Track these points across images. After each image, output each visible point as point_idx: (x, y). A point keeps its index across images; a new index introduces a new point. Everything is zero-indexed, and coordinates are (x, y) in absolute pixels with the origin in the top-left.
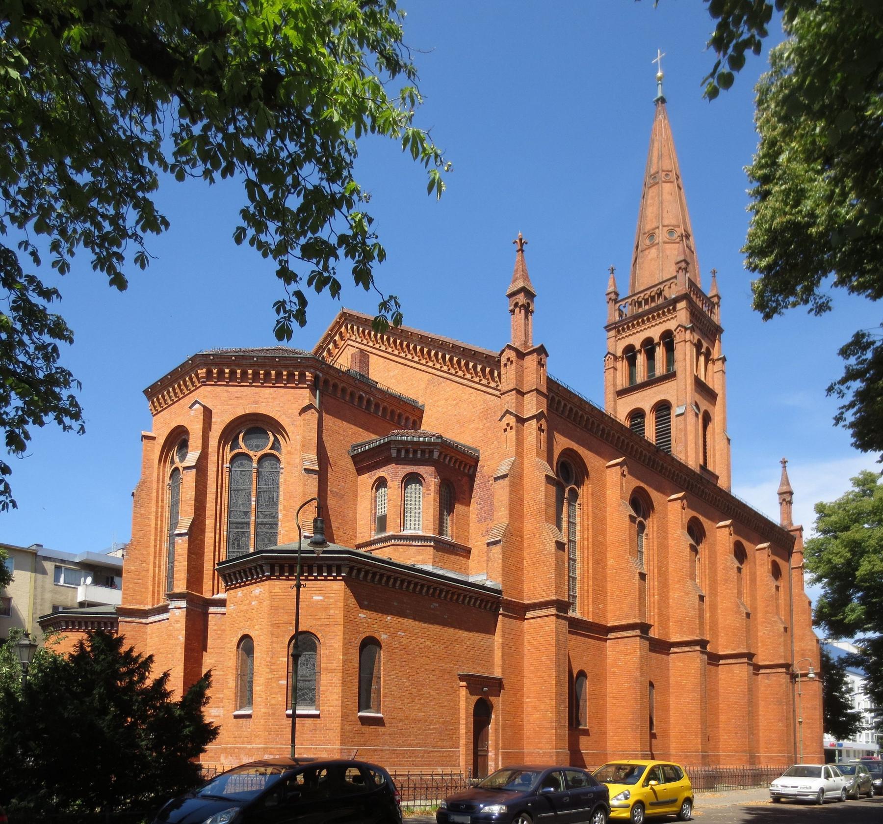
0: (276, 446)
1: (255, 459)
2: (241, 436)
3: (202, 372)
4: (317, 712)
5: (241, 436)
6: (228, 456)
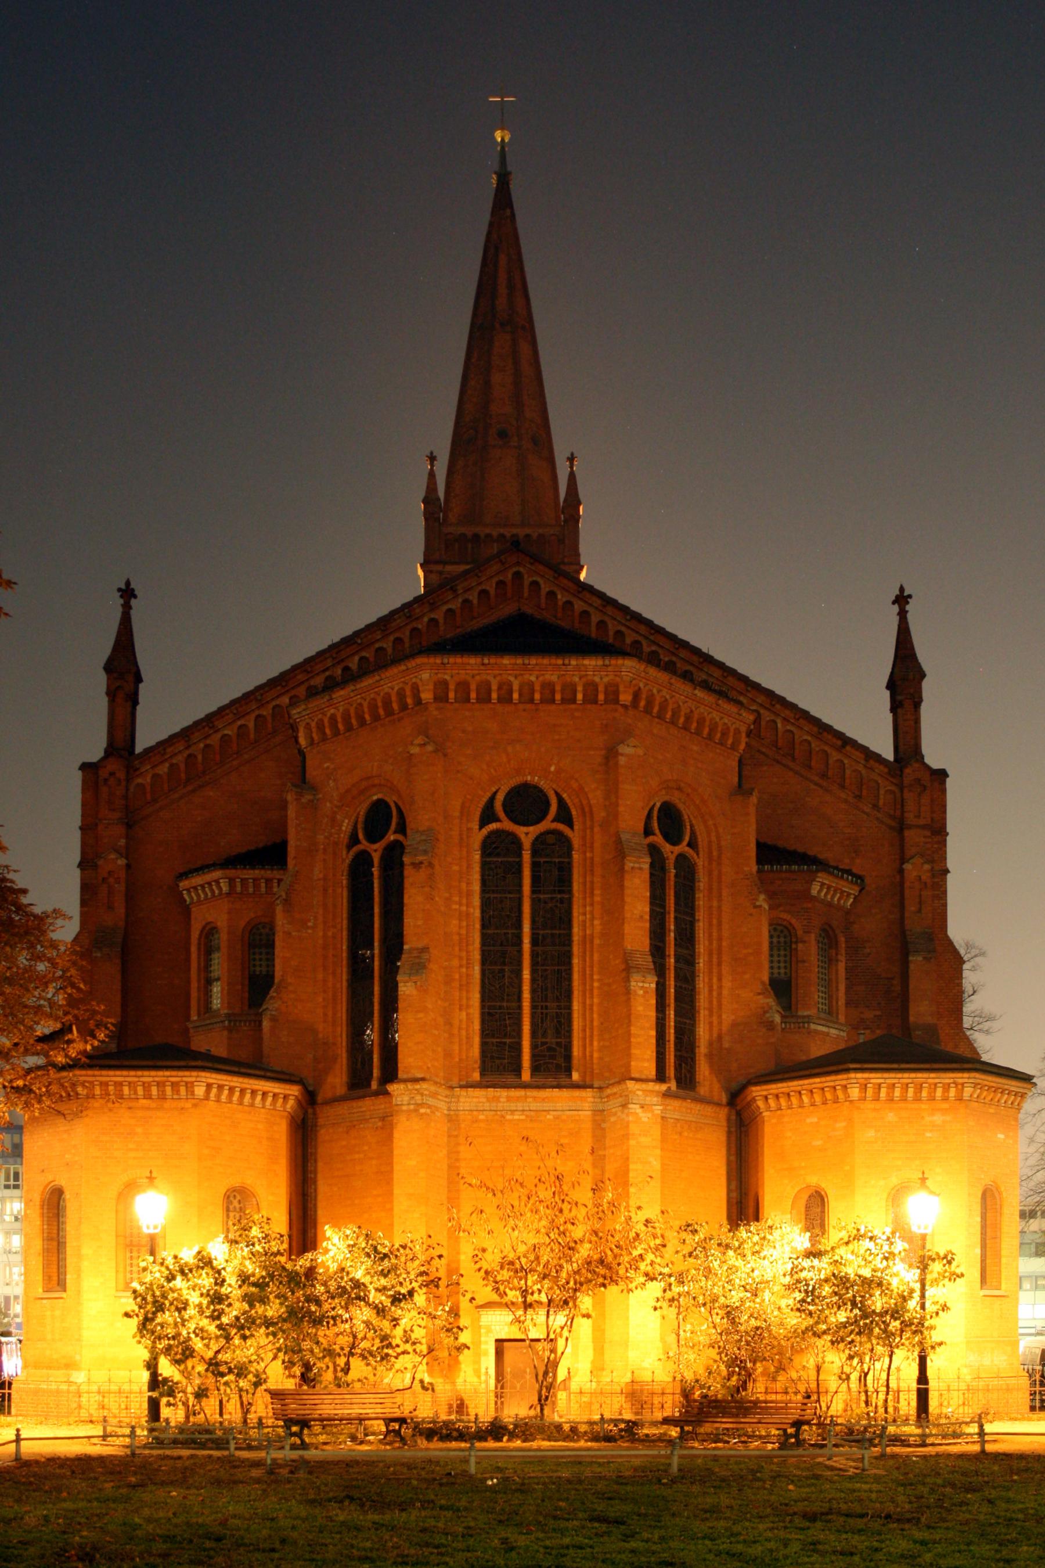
0: (565, 816)
6: (478, 836)
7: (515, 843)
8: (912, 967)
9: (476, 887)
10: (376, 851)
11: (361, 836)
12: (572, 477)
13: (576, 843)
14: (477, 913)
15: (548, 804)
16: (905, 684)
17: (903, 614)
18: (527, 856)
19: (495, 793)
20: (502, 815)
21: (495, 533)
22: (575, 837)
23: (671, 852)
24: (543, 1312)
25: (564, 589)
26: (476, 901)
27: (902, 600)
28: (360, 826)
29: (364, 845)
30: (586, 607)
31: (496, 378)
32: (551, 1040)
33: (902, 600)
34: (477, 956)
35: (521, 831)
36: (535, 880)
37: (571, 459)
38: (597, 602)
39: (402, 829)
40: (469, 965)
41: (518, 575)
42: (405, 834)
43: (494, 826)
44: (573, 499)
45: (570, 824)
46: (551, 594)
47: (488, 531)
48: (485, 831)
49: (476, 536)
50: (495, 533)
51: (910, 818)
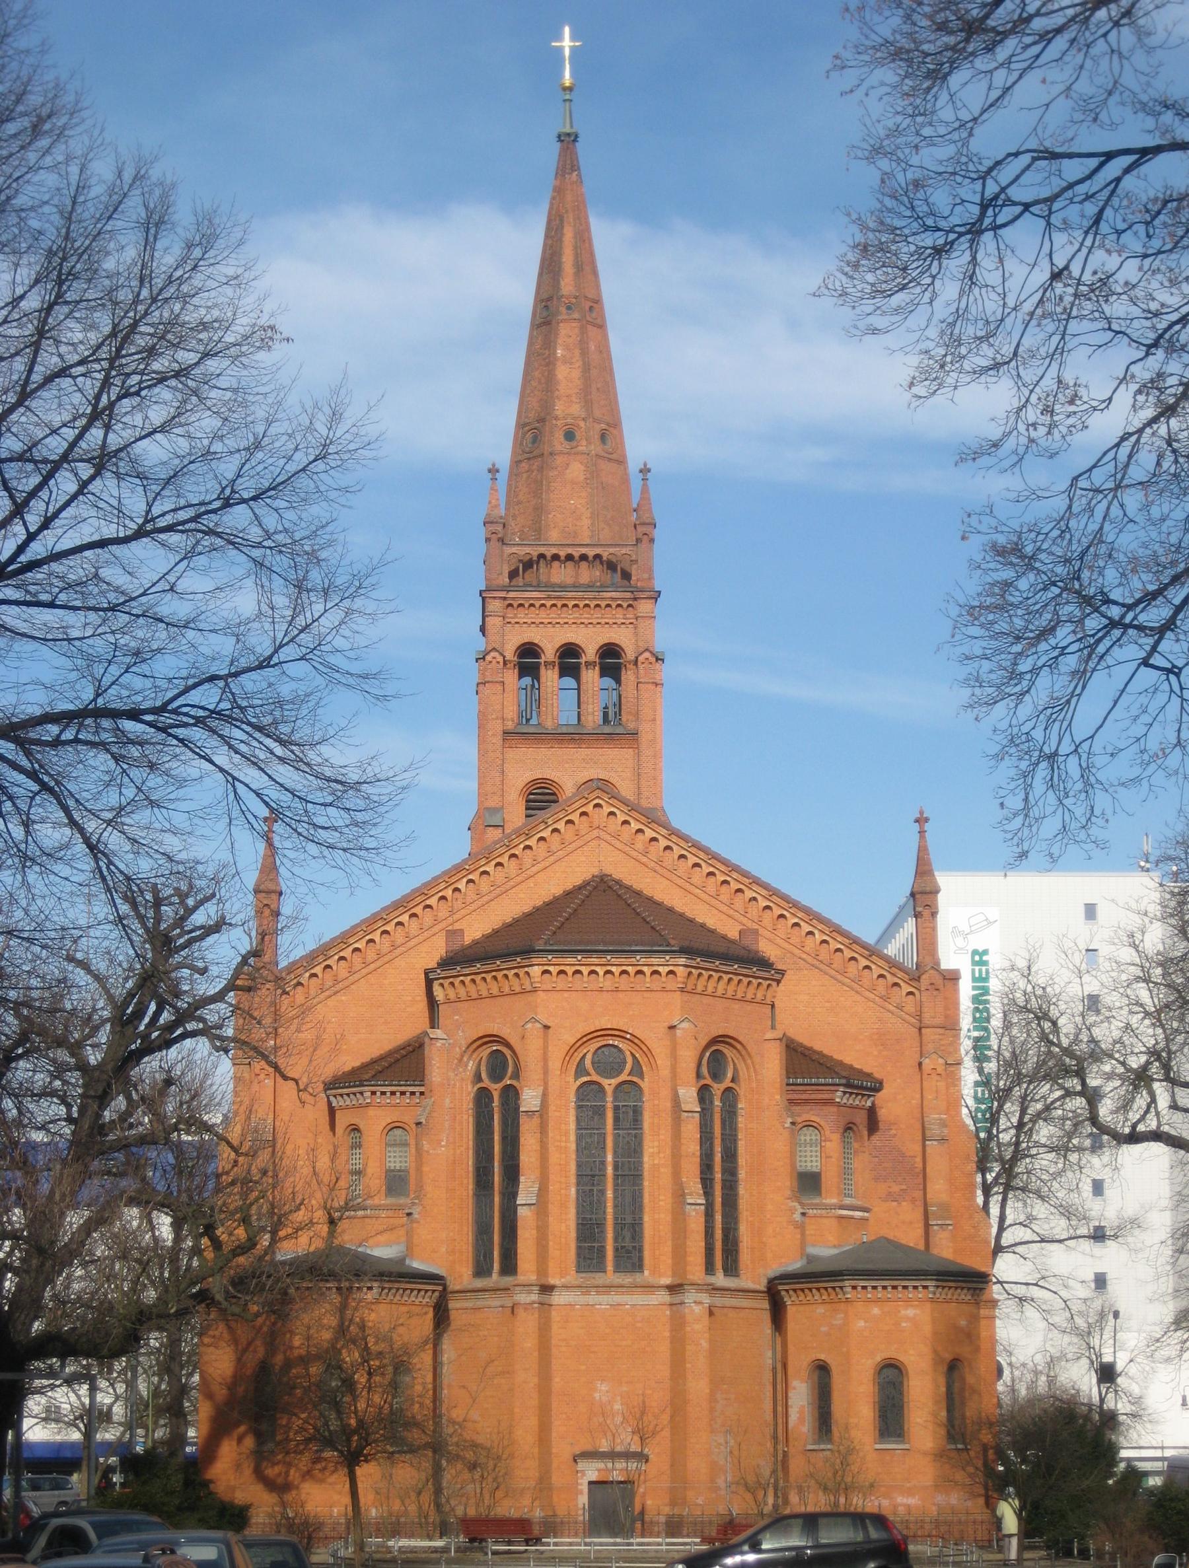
0: (637, 1070)
1: (609, 1090)
2: (589, 1056)
4: (907, 1446)
9: (572, 1126)
10: (495, 1088)
11: (484, 1075)
12: (645, 490)
13: (646, 1091)
14: (573, 1146)
18: (609, 1099)
20: (592, 1071)
21: (562, 554)
22: (645, 1085)
23: (717, 1089)
26: (573, 1138)
28: (483, 1063)
29: (486, 1082)
30: (654, 835)
31: (562, 372)
32: (628, 1243)
33: (921, 820)
34: (573, 1180)
35: (605, 1082)
36: (616, 1119)
39: (516, 1075)
40: (567, 1188)
45: (641, 1075)
48: (578, 1083)
50: (562, 554)
51: (927, 1019)
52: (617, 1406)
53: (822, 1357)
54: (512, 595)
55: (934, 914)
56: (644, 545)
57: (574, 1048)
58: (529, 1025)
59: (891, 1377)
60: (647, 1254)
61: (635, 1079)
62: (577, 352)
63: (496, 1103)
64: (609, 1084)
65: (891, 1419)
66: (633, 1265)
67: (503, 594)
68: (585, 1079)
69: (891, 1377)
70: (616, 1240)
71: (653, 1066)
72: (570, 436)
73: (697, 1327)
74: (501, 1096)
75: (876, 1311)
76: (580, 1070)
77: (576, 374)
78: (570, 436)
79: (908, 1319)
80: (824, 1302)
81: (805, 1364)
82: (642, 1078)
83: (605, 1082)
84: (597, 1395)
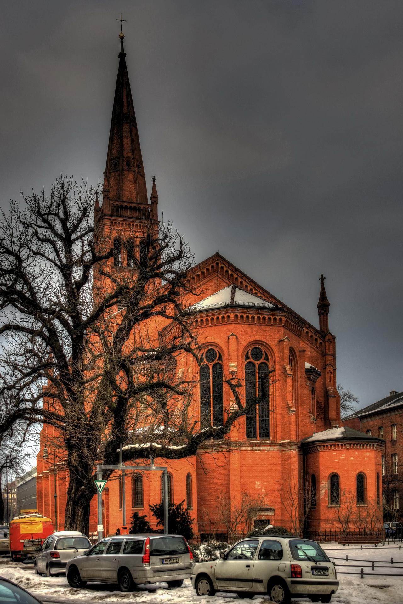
0: (267, 358)
2: (250, 352)
3: (232, 315)
5: (250, 352)
7: (254, 365)
8: (330, 400)
15: (262, 355)
16: (323, 307)
17: (323, 284)
19: (248, 352)
20: (251, 357)
24: (353, 517)
25: (231, 270)
27: (322, 279)
31: (125, 141)
33: (322, 279)
35: (256, 362)
37: (154, 179)
38: (241, 275)
41: (217, 264)
42: (222, 361)
43: (249, 361)
44: (155, 197)
45: (268, 360)
46: (227, 271)
47: (126, 204)
49: (122, 205)
52: (263, 491)
53: (336, 471)
54: (113, 218)
55: (327, 314)
56: (155, 205)
57: (246, 347)
58: (231, 337)
59: (361, 479)
60: (271, 431)
61: (266, 362)
62: (129, 135)
63: (211, 371)
64: (257, 363)
65: (361, 495)
66: (266, 435)
67: (110, 218)
68: (249, 361)
69: (361, 479)
70: (259, 425)
71: (273, 357)
72: (128, 164)
73: (294, 459)
74: (213, 368)
75: (357, 453)
76: (247, 358)
77: (129, 142)
78: (128, 164)
79: (367, 457)
80: (337, 450)
81: (328, 475)
82: (268, 362)
83: (256, 362)
84: (256, 486)
